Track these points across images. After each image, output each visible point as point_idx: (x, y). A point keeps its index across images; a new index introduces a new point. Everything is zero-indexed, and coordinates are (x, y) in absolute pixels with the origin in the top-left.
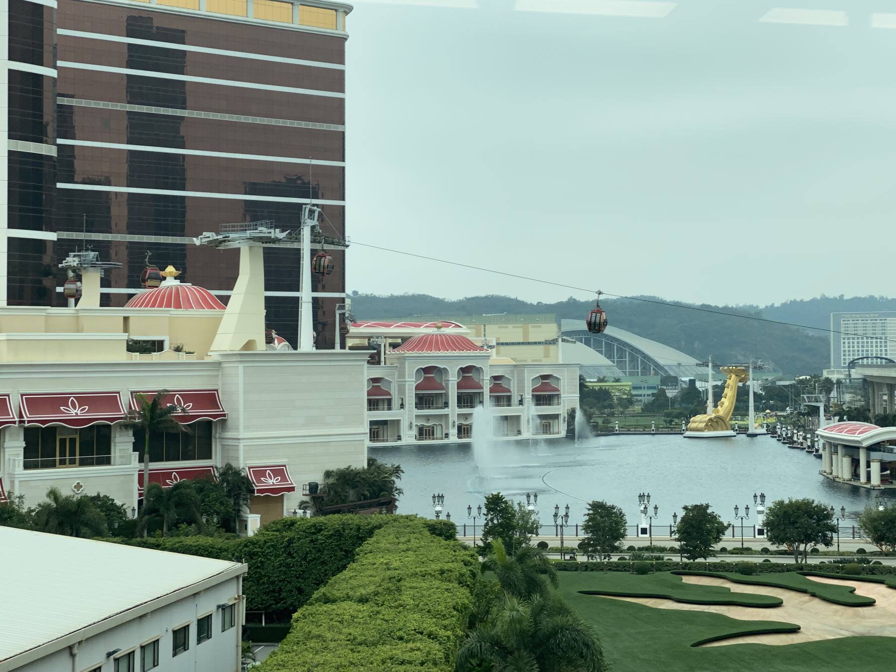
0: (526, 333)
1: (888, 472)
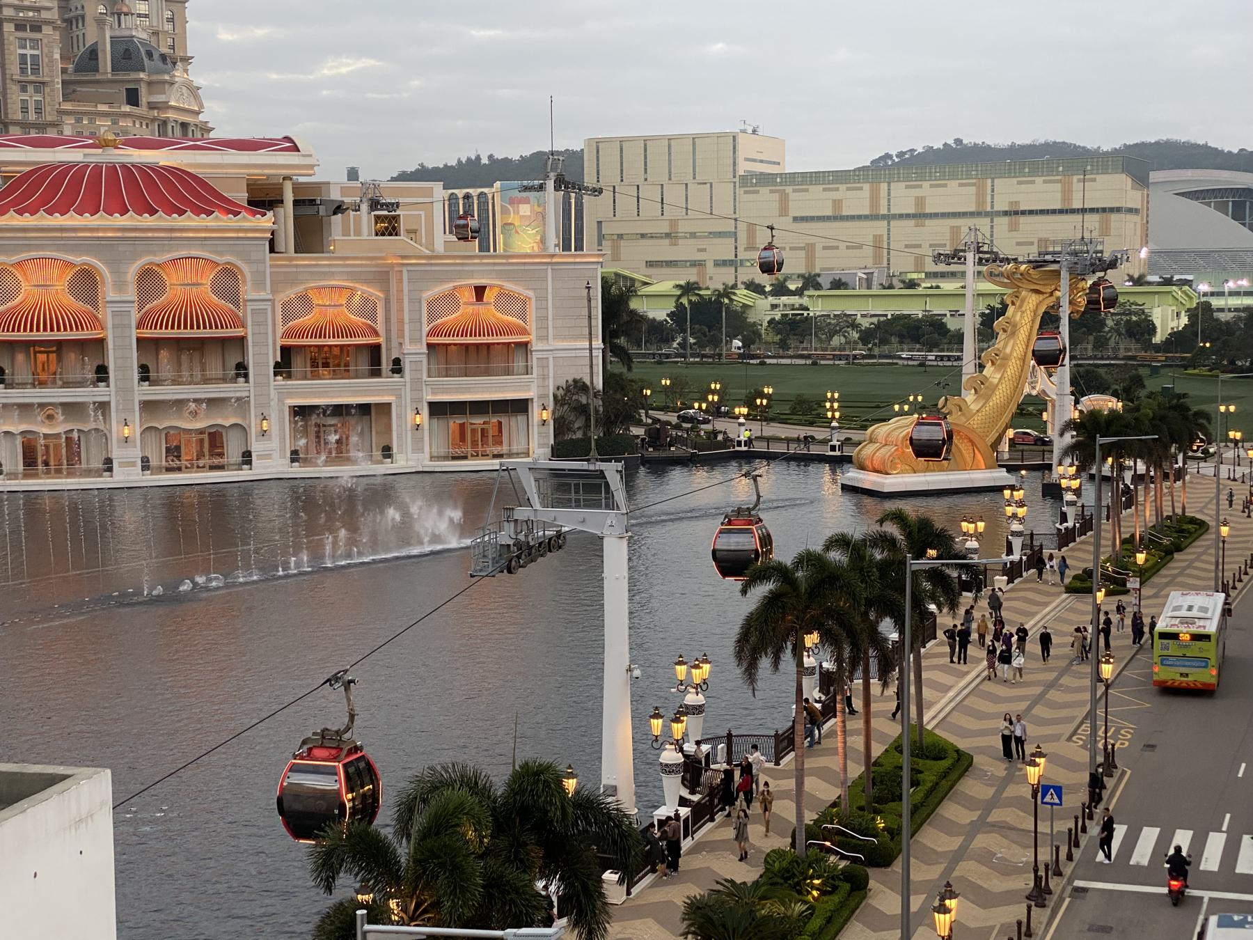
0: (1067, 193)
1: (393, 904)
